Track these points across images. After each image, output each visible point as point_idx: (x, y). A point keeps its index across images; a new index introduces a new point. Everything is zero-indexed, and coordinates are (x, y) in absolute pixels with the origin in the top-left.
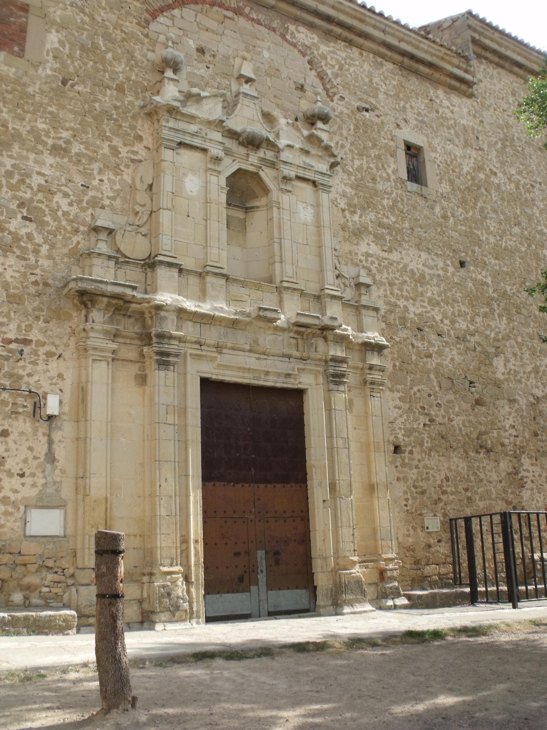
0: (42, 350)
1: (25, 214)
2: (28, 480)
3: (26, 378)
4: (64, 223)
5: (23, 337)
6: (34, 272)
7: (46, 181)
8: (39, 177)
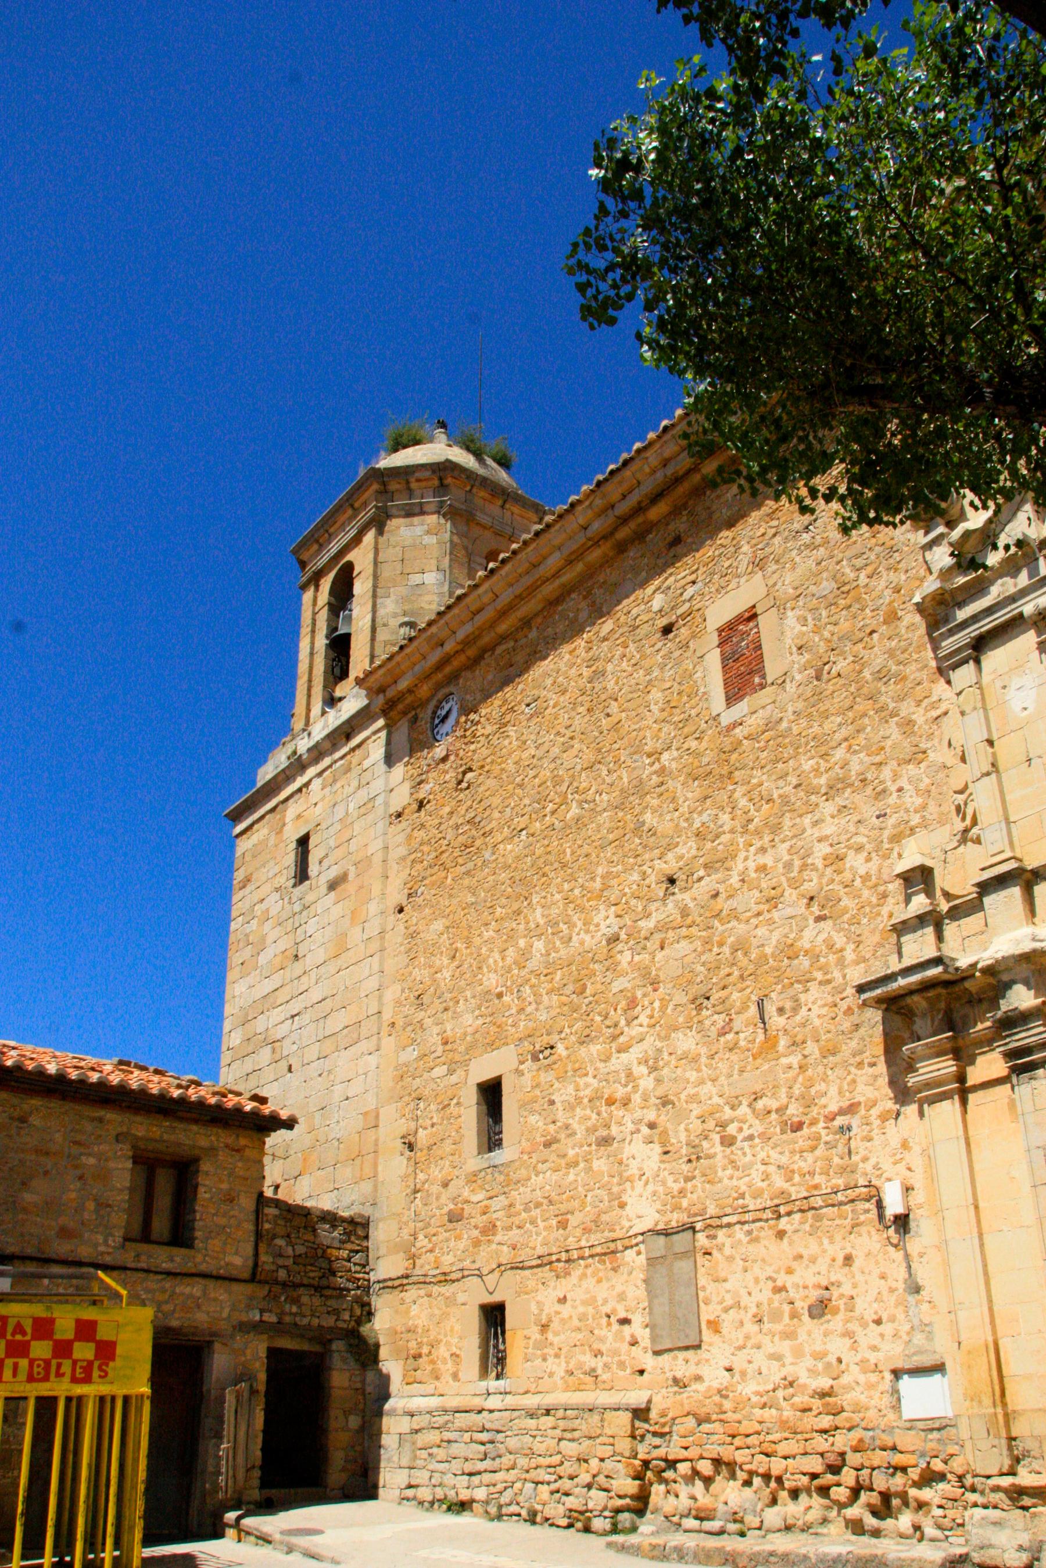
0: (874, 1112)
1: (818, 913)
2: (887, 1328)
3: (861, 1165)
4: (866, 893)
5: (848, 1103)
6: (844, 995)
7: (831, 845)
8: (822, 845)
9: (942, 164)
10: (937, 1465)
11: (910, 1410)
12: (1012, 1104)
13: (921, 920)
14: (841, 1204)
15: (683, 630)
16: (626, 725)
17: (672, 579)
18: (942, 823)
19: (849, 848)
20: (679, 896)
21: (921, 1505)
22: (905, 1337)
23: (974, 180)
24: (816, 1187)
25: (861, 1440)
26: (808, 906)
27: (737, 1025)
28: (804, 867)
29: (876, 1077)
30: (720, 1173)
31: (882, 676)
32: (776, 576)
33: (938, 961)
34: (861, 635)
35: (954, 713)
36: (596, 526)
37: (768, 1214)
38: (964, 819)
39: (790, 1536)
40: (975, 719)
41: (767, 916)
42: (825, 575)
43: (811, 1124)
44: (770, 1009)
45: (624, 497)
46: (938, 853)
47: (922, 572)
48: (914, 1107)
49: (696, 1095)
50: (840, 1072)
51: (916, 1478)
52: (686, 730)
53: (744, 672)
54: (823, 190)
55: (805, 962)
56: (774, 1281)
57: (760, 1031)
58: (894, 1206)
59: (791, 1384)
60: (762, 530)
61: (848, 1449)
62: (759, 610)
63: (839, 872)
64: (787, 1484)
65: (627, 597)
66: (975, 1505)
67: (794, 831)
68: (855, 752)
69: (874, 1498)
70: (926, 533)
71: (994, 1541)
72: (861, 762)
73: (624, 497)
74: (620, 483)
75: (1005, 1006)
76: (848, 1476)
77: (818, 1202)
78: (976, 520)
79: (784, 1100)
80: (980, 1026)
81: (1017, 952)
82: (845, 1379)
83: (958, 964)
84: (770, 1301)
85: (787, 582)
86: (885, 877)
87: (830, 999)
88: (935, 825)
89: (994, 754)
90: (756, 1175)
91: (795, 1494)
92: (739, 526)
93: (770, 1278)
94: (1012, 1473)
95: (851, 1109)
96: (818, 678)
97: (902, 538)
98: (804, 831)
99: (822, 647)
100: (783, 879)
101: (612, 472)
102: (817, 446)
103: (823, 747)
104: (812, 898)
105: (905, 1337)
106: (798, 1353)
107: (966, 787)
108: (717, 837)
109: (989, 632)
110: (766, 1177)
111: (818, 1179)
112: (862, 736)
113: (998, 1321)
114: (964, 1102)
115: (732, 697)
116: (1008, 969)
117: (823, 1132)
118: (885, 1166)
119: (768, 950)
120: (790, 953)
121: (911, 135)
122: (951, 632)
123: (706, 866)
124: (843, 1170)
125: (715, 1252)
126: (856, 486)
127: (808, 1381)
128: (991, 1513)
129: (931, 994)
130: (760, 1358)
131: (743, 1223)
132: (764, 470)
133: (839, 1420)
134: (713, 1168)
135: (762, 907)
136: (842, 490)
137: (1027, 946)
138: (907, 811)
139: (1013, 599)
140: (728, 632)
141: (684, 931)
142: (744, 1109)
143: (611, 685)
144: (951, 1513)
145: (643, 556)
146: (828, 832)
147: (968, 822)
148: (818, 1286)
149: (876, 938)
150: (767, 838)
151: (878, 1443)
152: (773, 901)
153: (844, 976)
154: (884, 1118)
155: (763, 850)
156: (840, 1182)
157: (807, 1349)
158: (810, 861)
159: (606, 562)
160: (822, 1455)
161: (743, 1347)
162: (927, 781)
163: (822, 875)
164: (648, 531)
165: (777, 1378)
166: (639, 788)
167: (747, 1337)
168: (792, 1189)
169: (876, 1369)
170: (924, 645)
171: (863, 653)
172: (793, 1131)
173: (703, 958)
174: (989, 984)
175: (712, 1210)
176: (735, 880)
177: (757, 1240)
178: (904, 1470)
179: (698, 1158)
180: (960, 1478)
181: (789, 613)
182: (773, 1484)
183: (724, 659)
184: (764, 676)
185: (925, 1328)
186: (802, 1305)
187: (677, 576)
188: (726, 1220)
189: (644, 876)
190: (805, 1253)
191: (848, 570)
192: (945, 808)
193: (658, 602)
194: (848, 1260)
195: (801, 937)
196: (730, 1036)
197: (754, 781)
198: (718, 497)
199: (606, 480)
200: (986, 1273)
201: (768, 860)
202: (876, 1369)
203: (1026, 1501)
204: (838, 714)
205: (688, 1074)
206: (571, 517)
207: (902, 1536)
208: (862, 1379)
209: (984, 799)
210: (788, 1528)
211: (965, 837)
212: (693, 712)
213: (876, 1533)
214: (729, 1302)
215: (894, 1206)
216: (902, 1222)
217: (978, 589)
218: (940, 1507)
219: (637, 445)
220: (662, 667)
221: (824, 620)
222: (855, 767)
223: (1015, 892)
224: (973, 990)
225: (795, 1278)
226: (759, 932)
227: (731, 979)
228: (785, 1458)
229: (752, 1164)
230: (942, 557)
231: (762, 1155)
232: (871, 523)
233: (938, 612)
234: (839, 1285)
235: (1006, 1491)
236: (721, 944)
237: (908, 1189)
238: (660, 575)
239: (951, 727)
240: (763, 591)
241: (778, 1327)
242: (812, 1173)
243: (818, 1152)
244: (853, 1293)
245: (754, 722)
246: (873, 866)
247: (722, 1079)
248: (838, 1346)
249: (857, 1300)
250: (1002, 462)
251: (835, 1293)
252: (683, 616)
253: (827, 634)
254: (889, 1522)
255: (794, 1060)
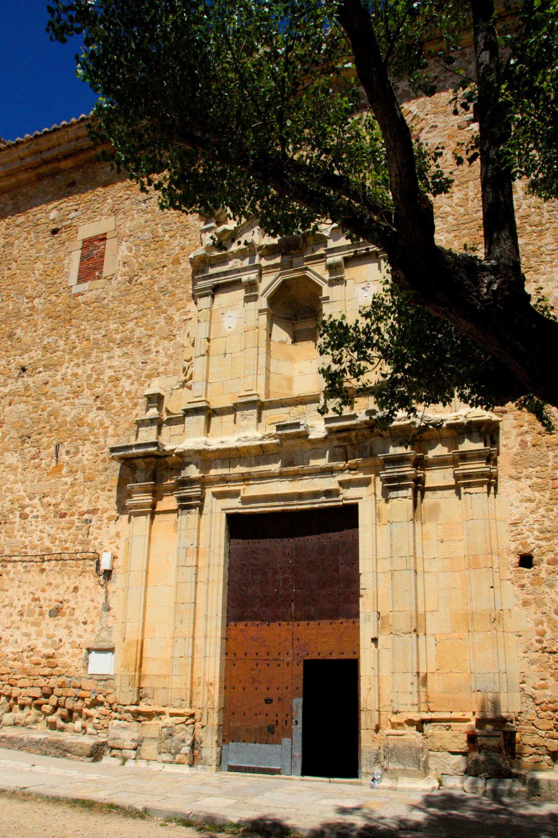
0: (106, 515)
2: (89, 627)
4: (127, 401)
8: (110, 370)
9: (261, 36)
10: (101, 698)
11: (92, 669)
12: (176, 524)
13: (152, 422)
14: (78, 559)
15: (63, 235)
16: (18, 278)
17: (64, 205)
18: (175, 373)
19: (124, 375)
20: (26, 379)
21: (88, 717)
22: (97, 633)
23: (274, 50)
24: (67, 549)
25: (64, 682)
26: (95, 400)
27: (42, 455)
28: (97, 380)
29: (110, 497)
30: (16, 533)
31: (163, 290)
32: (122, 221)
33: (155, 444)
34: (158, 266)
35: (195, 320)
36: (29, 160)
37: (38, 559)
38: (186, 375)
39: (16, 728)
40: (204, 326)
41: (72, 400)
42: (148, 229)
43: (71, 515)
44: (62, 450)
45: (49, 149)
46: (168, 389)
47: (198, 243)
48: (126, 517)
49: (12, 488)
50: (92, 491)
51: (88, 703)
52: (51, 289)
53: (91, 267)
54: (199, 21)
55: (86, 430)
56: (34, 594)
57: (54, 461)
58: (105, 565)
59: (32, 650)
60: (121, 194)
61: (56, 686)
62: (108, 236)
63: (115, 387)
64: (19, 702)
65: (37, 206)
66: (116, 718)
67: (97, 359)
68: (139, 326)
69: (64, 712)
70: (205, 224)
71: (121, 736)
72: (141, 332)
73: (49, 149)
74: (49, 140)
75: (184, 474)
76: (53, 700)
77: (66, 557)
78: (231, 225)
79: (59, 500)
80: (169, 482)
81: (196, 448)
82: (61, 651)
83: (165, 448)
84: (30, 605)
85: (127, 226)
86: (139, 395)
87: (95, 452)
88: (171, 374)
89: (209, 346)
90: (35, 537)
91: (22, 707)
92: (109, 188)
93: (31, 593)
94: (137, 704)
95: (94, 511)
96: (130, 282)
97: (192, 223)
98: (102, 360)
99: (137, 266)
100: (85, 383)
101: (46, 133)
102: (158, 157)
103: (123, 319)
104: (98, 397)
105: (97, 633)
106: (39, 634)
107: (191, 359)
108: (55, 352)
109: (222, 284)
110: (41, 539)
111: (68, 545)
112: (145, 319)
113: (146, 630)
114: (152, 518)
115: (81, 279)
116: (189, 456)
117: (76, 521)
118: (105, 544)
119: (68, 419)
120: (80, 423)
121: (250, 12)
122: (204, 278)
123: (44, 366)
124: (82, 542)
125: (4, 575)
126: (173, 186)
127: (42, 649)
128: (123, 723)
129: (148, 460)
130: (18, 635)
131: (23, 562)
132: (127, 160)
133: (54, 671)
134: (13, 530)
135: (70, 395)
136: (165, 186)
137: (201, 447)
138: (158, 364)
139: (238, 271)
140: (88, 243)
141: (24, 398)
142: (36, 501)
143: (15, 252)
144: (102, 722)
145: (52, 186)
146: (115, 364)
147: (188, 377)
148: (57, 601)
149: (127, 425)
150: (81, 360)
151: (72, 684)
152: (77, 394)
153: (105, 442)
154: (110, 519)
155: (78, 365)
156: (80, 548)
157: (44, 633)
158: (101, 377)
159: (29, 182)
160: (41, 688)
161: (10, 627)
162: (172, 351)
163: (106, 386)
164: (59, 173)
165: (25, 646)
166: (17, 314)
167: (13, 622)
168: (54, 548)
169: (79, 647)
170: (188, 281)
171: (157, 275)
172: (61, 517)
173: (32, 415)
174: (179, 462)
175: (7, 552)
176: (59, 377)
177: (29, 571)
178: (83, 699)
179: (5, 523)
180: (111, 705)
181: (124, 243)
182: (12, 701)
183: (82, 257)
184: (101, 273)
185: (109, 629)
186: (46, 609)
187: (68, 204)
188: (14, 558)
189: (9, 363)
190: (54, 582)
191: (160, 230)
192: (178, 367)
193: (53, 215)
194: (76, 589)
195: (87, 416)
196: (37, 461)
197: (82, 327)
198: (102, 168)
199: (41, 136)
200: (145, 606)
201: (79, 371)
202: (79, 647)
203: (141, 718)
204: (134, 304)
205: (9, 476)
206: (14, 149)
207: (75, 731)
208: (71, 651)
209: (198, 368)
210: (15, 724)
211: (184, 384)
212: (58, 281)
213: (62, 729)
214: (7, 602)
215: (105, 565)
216: (108, 574)
217: (224, 260)
218: (98, 718)
219: (64, 123)
220: (47, 251)
221: (141, 253)
222: (137, 334)
223: (202, 418)
224: (170, 463)
225: (46, 595)
226: (66, 408)
227: (44, 430)
228: (21, 688)
229: (34, 531)
230: (207, 239)
231: (41, 527)
232: (176, 208)
233: (200, 266)
234: (68, 601)
235: (132, 713)
236: (43, 410)
237: (114, 558)
238: (58, 200)
239: (191, 327)
240: (112, 227)
241: (31, 619)
242: (66, 541)
243: (72, 531)
244: (75, 606)
245: (90, 296)
246: (134, 388)
247: (28, 483)
248: (61, 633)
249: (76, 611)
250: (249, 200)
251: (66, 605)
252: (66, 227)
253: (140, 260)
254: (70, 724)
255: (69, 480)
